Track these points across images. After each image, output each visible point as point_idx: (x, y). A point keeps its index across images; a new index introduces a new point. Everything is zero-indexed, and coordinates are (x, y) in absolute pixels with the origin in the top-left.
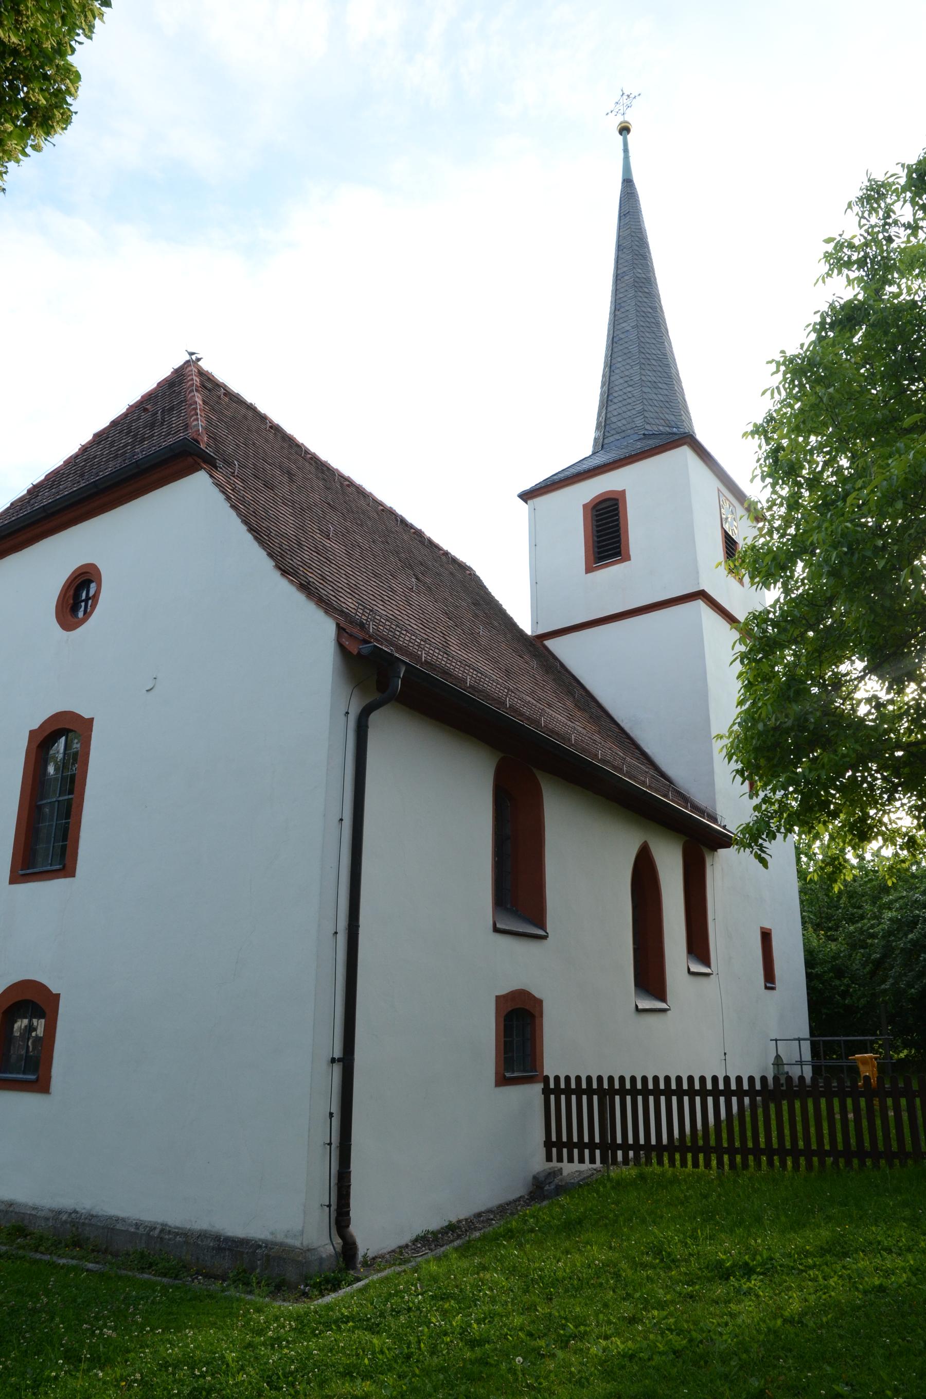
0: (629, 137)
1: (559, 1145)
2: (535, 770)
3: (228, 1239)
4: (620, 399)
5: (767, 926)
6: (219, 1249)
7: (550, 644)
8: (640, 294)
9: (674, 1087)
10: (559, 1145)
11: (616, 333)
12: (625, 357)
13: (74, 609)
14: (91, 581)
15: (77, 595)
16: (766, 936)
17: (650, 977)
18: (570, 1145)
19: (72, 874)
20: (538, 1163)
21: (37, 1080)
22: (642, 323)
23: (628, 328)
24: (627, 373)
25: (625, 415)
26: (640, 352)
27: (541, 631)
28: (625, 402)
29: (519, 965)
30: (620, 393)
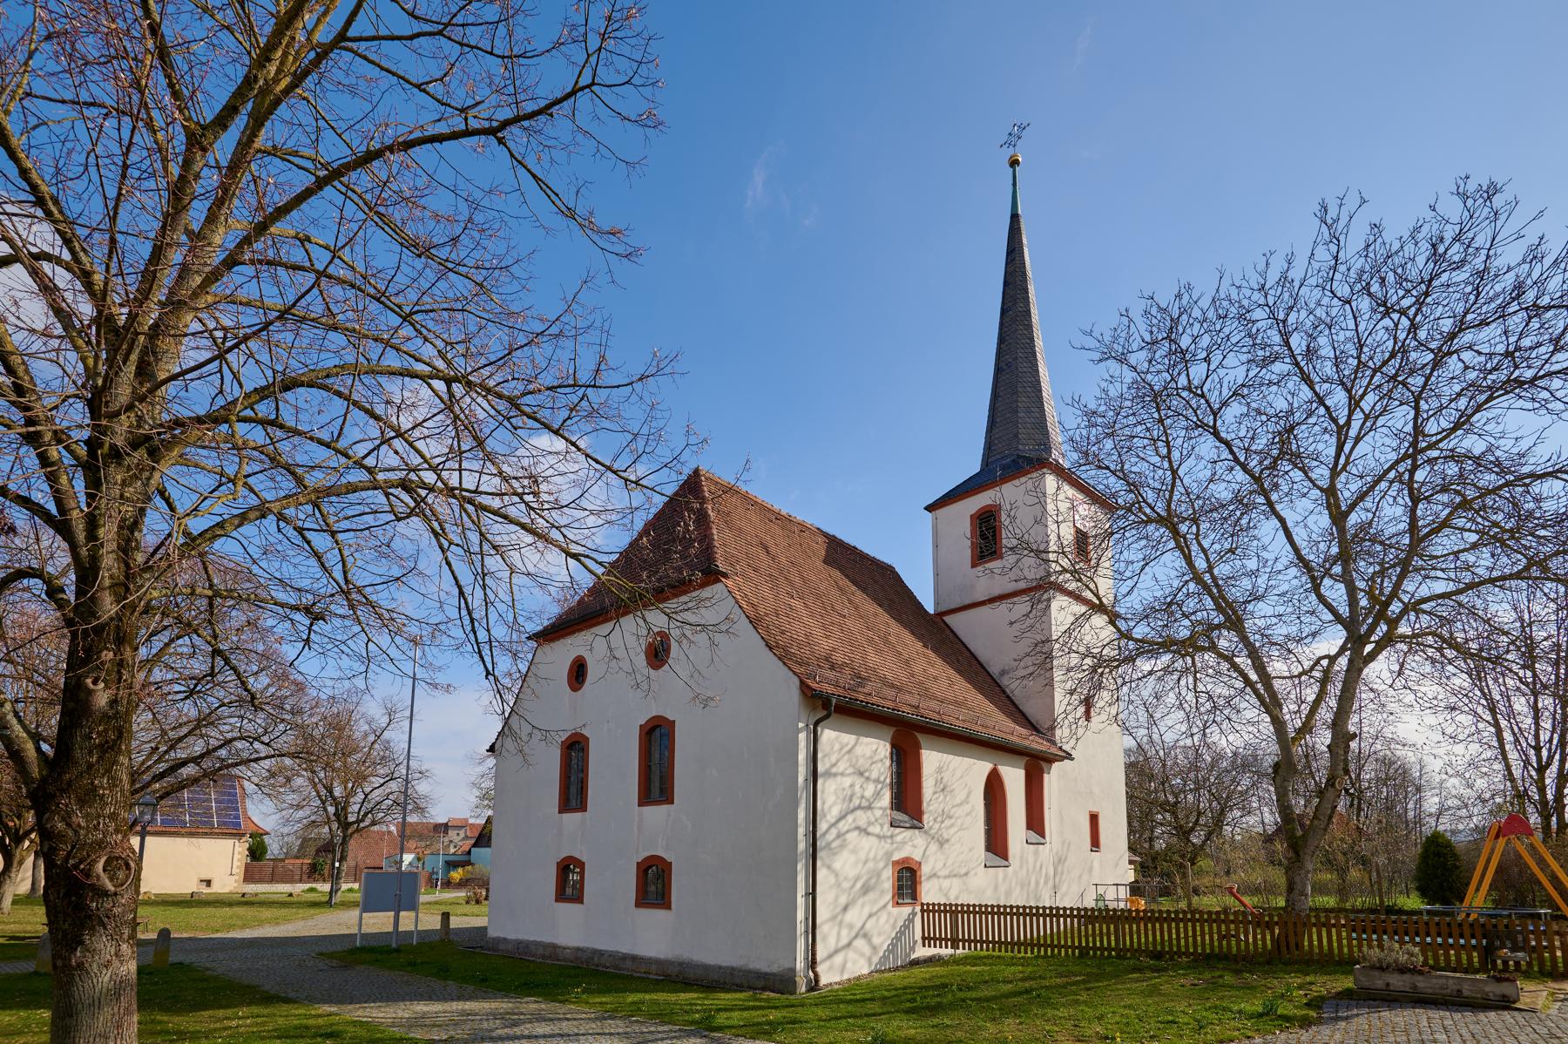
1: (930, 939)
5: (1095, 810)
16: (1094, 818)
17: (996, 843)
18: (935, 939)
19: (585, 810)
27: (942, 609)
29: (911, 845)
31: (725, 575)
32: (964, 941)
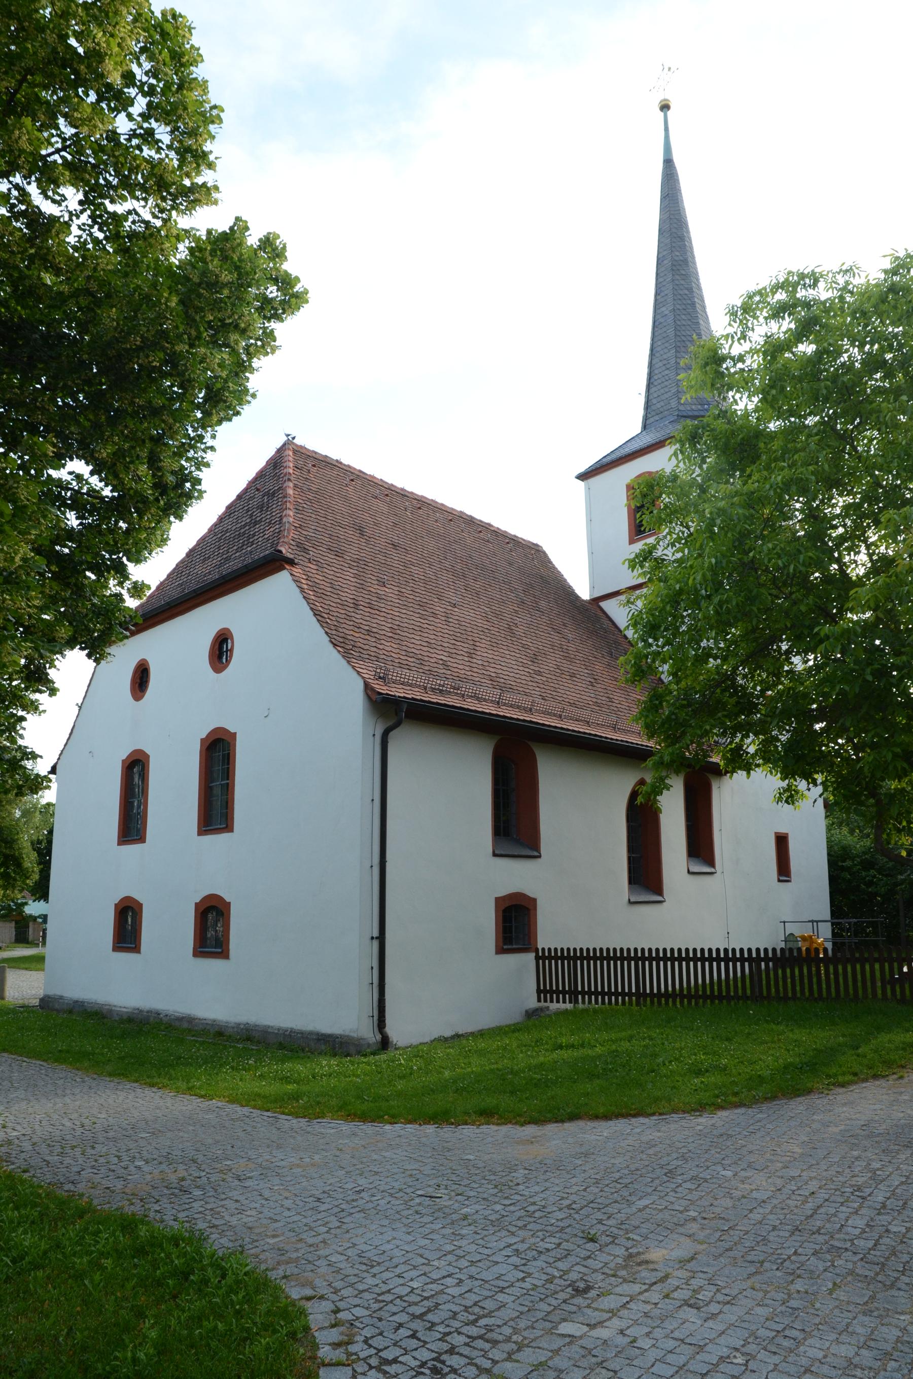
0: (669, 113)
2: (529, 743)
3: (323, 1035)
4: (659, 381)
5: (782, 830)
6: (318, 1040)
7: (603, 604)
8: (678, 277)
9: (714, 955)
10: (545, 992)
11: (657, 317)
12: (664, 341)
13: (220, 657)
14: (227, 639)
15: (221, 648)
16: (782, 841)
17: (645, 874)
19: (232, 831)
20: (532, 1002)
21: (222, 952)
22: (678, 306)
23: (667, 312)
24: (665, 357)
25: (663, 397)
26: (676, 335)
28: (663, 385)
29: (516, 876)
30: (660, 376)
31: (291, 562)
32: (583, 993)
